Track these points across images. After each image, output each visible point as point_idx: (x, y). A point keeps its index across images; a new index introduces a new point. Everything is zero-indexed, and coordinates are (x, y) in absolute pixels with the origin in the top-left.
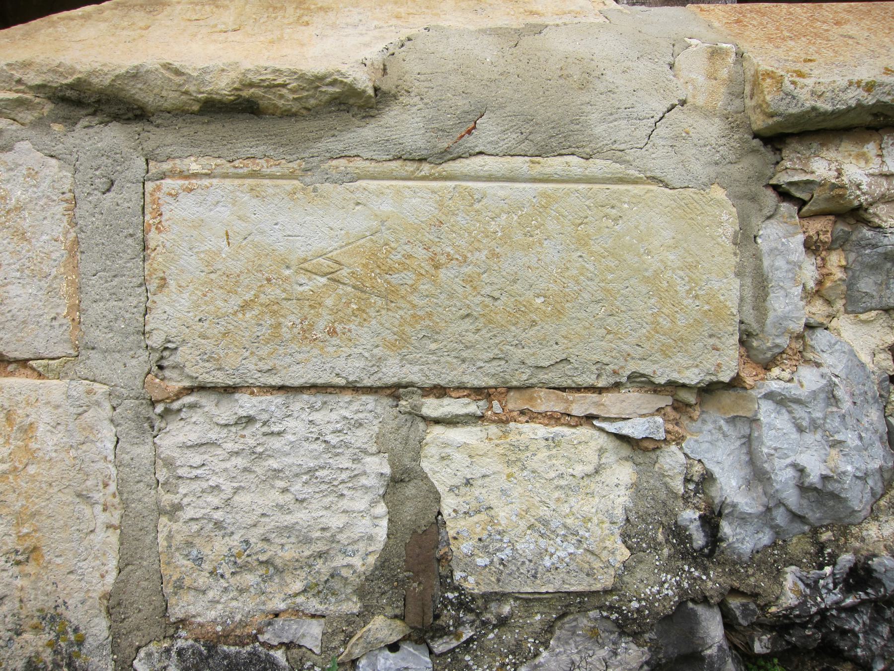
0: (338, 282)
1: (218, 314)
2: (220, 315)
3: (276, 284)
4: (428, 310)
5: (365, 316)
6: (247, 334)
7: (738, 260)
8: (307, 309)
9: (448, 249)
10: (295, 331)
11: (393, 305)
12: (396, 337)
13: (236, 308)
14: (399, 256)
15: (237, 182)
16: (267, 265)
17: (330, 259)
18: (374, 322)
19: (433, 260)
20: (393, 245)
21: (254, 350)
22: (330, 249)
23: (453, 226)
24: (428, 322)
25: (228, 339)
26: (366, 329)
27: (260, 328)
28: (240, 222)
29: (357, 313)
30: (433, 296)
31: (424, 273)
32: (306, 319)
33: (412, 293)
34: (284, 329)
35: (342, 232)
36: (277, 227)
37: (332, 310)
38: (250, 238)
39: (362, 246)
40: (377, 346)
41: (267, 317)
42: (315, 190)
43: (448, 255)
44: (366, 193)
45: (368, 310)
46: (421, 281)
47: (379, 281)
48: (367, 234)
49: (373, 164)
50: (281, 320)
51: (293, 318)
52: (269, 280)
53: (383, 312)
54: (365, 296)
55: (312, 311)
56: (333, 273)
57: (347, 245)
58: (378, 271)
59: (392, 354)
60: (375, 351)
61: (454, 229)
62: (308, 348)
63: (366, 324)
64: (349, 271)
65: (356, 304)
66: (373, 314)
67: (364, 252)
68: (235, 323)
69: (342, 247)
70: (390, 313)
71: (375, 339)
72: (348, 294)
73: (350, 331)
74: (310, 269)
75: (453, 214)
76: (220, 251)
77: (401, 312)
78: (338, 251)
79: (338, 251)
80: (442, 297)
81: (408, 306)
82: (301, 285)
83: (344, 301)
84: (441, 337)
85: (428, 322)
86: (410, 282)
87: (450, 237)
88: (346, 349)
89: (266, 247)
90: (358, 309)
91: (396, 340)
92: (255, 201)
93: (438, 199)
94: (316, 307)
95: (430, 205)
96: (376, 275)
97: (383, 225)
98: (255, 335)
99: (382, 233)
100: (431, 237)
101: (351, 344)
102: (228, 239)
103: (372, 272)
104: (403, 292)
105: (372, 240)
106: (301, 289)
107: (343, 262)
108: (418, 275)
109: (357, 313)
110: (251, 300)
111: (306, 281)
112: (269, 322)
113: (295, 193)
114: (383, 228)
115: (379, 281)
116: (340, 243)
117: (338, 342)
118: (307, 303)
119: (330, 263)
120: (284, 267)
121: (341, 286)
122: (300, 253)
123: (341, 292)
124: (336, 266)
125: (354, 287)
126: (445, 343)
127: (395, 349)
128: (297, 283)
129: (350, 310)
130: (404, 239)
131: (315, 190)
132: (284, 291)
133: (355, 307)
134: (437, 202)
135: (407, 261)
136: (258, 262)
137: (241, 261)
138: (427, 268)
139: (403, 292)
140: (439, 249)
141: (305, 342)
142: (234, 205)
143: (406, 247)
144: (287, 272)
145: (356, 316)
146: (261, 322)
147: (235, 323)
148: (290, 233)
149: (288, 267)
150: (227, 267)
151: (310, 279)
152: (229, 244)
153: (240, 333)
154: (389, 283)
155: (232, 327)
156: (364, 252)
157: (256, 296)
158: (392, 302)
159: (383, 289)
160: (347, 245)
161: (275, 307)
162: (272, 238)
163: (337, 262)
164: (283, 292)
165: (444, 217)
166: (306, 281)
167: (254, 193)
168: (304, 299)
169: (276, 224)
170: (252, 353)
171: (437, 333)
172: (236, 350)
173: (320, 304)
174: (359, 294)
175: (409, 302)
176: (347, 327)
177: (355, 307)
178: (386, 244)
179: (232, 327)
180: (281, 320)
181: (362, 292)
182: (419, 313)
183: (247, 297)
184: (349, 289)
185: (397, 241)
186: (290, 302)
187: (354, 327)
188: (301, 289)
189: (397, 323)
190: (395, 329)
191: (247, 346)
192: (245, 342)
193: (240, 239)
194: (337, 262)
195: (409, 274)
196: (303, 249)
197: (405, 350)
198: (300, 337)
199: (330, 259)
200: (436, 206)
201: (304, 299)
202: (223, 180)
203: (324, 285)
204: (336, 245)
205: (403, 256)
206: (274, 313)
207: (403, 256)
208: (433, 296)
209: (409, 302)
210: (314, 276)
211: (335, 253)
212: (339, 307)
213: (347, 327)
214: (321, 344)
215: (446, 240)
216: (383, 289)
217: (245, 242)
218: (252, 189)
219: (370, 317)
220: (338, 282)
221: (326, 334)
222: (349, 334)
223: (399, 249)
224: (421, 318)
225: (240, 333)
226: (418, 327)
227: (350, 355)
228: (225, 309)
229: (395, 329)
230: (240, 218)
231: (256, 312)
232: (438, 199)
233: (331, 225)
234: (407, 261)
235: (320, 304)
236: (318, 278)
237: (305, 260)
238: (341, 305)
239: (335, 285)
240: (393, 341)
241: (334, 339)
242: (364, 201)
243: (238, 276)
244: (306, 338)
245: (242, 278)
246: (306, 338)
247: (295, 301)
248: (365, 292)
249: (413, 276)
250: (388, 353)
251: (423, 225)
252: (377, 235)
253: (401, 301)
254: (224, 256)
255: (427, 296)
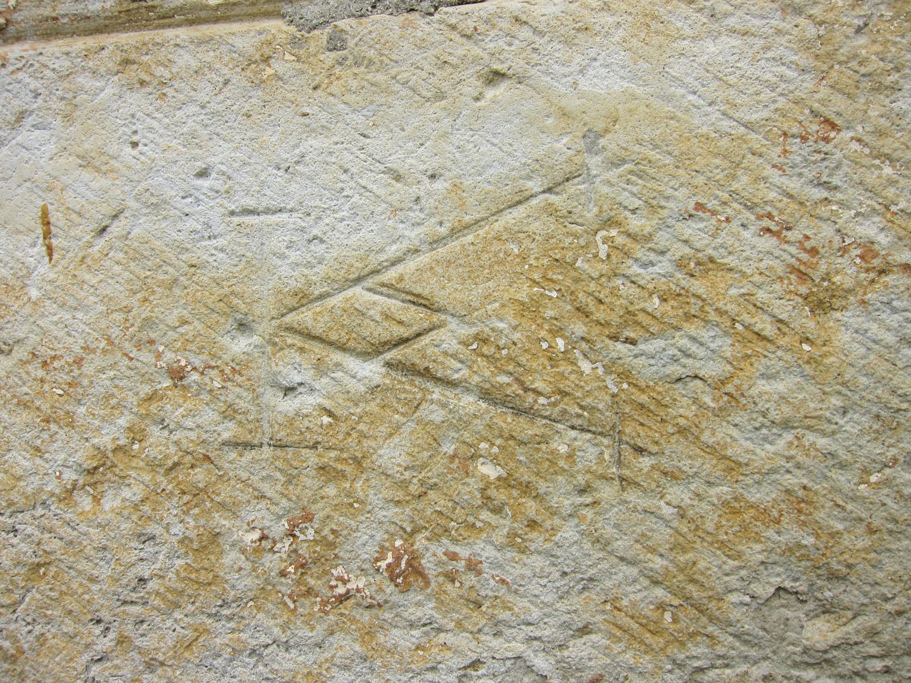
0: (426, 373)
1: (15, 496)
2: (20, 501)
3: (201, 387)
4: (791, 481)
5: (531, 507)
6: (105, 571)
7: (572, 326)
8: (309, 481)
9: (868, 230)
10: (271, 562)
11: (646, 462)
12: (659, 592)
13: (70, 476)
14: (664, 266)
15: (80, 44)
16: (172, 319)
17: (392, 289)
18: (568, 532)
19: (803, 276)
20: (635, 223)
21: (129, 629)
22: (393, 251)
23: (880, 133)
24: (792, 533)
25: (43, 586)
26: (538, 562)
27: (149, 548)
28: (86, 175)
29: (500, 496)
30: (812, 422)
31: (769, 330)
32: (308, 518)
33: (721, 413)
34: (231, 557)
35: (439, 185)
36: (204, 183)
37: (404, 485)
38: (116, 229)
39: (514, 234)
40: (585, 630)
41: (171, 509)
42: (336, 43)
43: (868, 251)
44: (525, 33)
45: (542, 486)
46: (760, 365)
47: (586, 366)
48: (534, 185)
49: (521, 208)
50: (221, 521)
51: (259, 513)
52: (177, 375)
53: (607, 492)
54: (528, 429)
55: (331, 490)
56: (404, 341)
57: (454, 233)
58: (579, 328)
59: (646, 662)
60: (578, 649)
61: (888, 145)
62: (320, 629)
63: (537, 540)
64: (466, 331)
65: (495, 460)
66: (567, 503)
67: (523, 258)
68: (65, 531)
69: (436, 242)
70: (632, 496)
71: (576, 601)
72: (463, 423)
73: (473, 566)
74: (318, 331)
75: (878, 88)
76: (25, 275)
77: (678, 493)
78: (424, 259)
79: (424, 259)
80: (850, 425)
81: (709, 465)
82: (289, 390)
83: (449, 448)
84: (852, 596)
85: (792, 533)
86: (713, 369)
87: (871, 178)
88: (462, 640)
89: (170, 255)
90: (505, 482)
91: (661, 607)
92: (136, 100)
93: (812, 31)
94: (343, 475)
95: (780, 61)
96: (572, 344)
97: (592, 149)
98: (131, 574)
99: (591, 179)
100: (793, 185)
101: (478, 619)
102: (47, 235)
103: (556, 332)
104: (685, 411)
105: (551, 211)
106: (288, 405)
107: (440, 297)
108: (743, 340)
109: (500, 496)
110: (117, 449)
111: (307, 376)
112: (177, 529)
113: (266, 60)
114: (594, 162)
115: (586, 366)
116: (431, 228)
117: (429, 610)
118: (312, 458)
119: (394, 305)
120: (230, 324)
121: (437, 393)
122: (285, 270)
123: (438, 415)
124: (416, 316)
125: (486, 395)
126: (869, 620)
127: (657, 642)
128: (275, 385)
129: (474, 484)
130: (683, 199)
131: (336, 43)
132: (230, 413)
133: (490, 471)
134: (806, 45)
135: (698, 286)
136: (141, 313)
137: (86, 309)
138: (783, 310)
139: (685, 411)
140: (827, 231)
141: (306, 606)
142: (68, 118)
143: (689, 229)
144: (241, 345)
145: (497, 510)
146: (153, 529)
147: (65, 531)
148: (251, 203)
149: (243, 327)
150: (44, 332)
151: (320, 367)
152: (50, 250)
153: (83, 565)
154: (625, 375)
155: (56, 544)
156: (524, 259)
157: (136, 434)
158: (640, 450)
159: (602, 402)
160: (454, 233)
161: (200, 475)
162: (191, 224)
163: (419, 301)
164: (225, 416)
165: (839, 102)
166: (307, 376)
167: (133, 72)
168: (297, 445)
169: (203, 174)
170: (122, 640)
171: (834, 577)
172: (69, 627)
173: (358, 462)
174: (506, 421)
175: (711, 450)
176: (464, 552)
177: (490, 471)
178: (610, 223)
179: (56, 544)
180: (221, 521)
181: (519, 411)
182: (754, 496)
183: (106, 439)
184: (469, 402)
185: (653, 208)
186: (249, 455)
187: (489, 552)
188: (288, 405)
189: (662, 535)
190: (658, 563)
191: (105, 615)
192: (99, 600)
193: (84, 231)
194: (419, 301)
195: (705, 335)
196: (294, 256)
197: (699, 650)
198: (286, 586)
199: (392, 289)
200: (803, 59)
201: (297, 445)
202: (40, 46)
203: (374, 389)
204: (413, 235)
205: (680, 264)
206: (198, 494)
207: (680, 264)
208: (812, 422)
209: (711, 450)
210: (337, 356)
211: (410, 265)
212: (433, 474)
213: (464, 552)
214: (366, 617)
215: (852, 193)
216: (602, 402)
217: (101, 243)
218: (127, 62)
219: (553, 512)
220: (426, 373)
221: (382, 579)
222: (470, 579)
223: (662, 239)
224: (763, 514)
225: (83, 565)
226: (754, 552)
227: (475, 664)
228: (36, 481)
229: (658, 563)
230: (86, 162)
231: (133, 492)
232: (812, 31)
233: (394, 162)
234: (698, 286)
235: (358, 462)
236: (352, 363)
237: (303, 299)
238: (438, 467)
239: (412, 388)
240: (649, 611)
241: (416, 596)
242: (518, 65)
243: (79, 362)
244: (310, 592)
245: (88, 369)
246: (310, 592)
247: (267, 452)
248: (529, 413)
249: (725, 346)
250: (628, 658)
251: (756, 140)
252: (572, 188)
253: (678, 445)
254: (34, 293)
255: (786, 425)
